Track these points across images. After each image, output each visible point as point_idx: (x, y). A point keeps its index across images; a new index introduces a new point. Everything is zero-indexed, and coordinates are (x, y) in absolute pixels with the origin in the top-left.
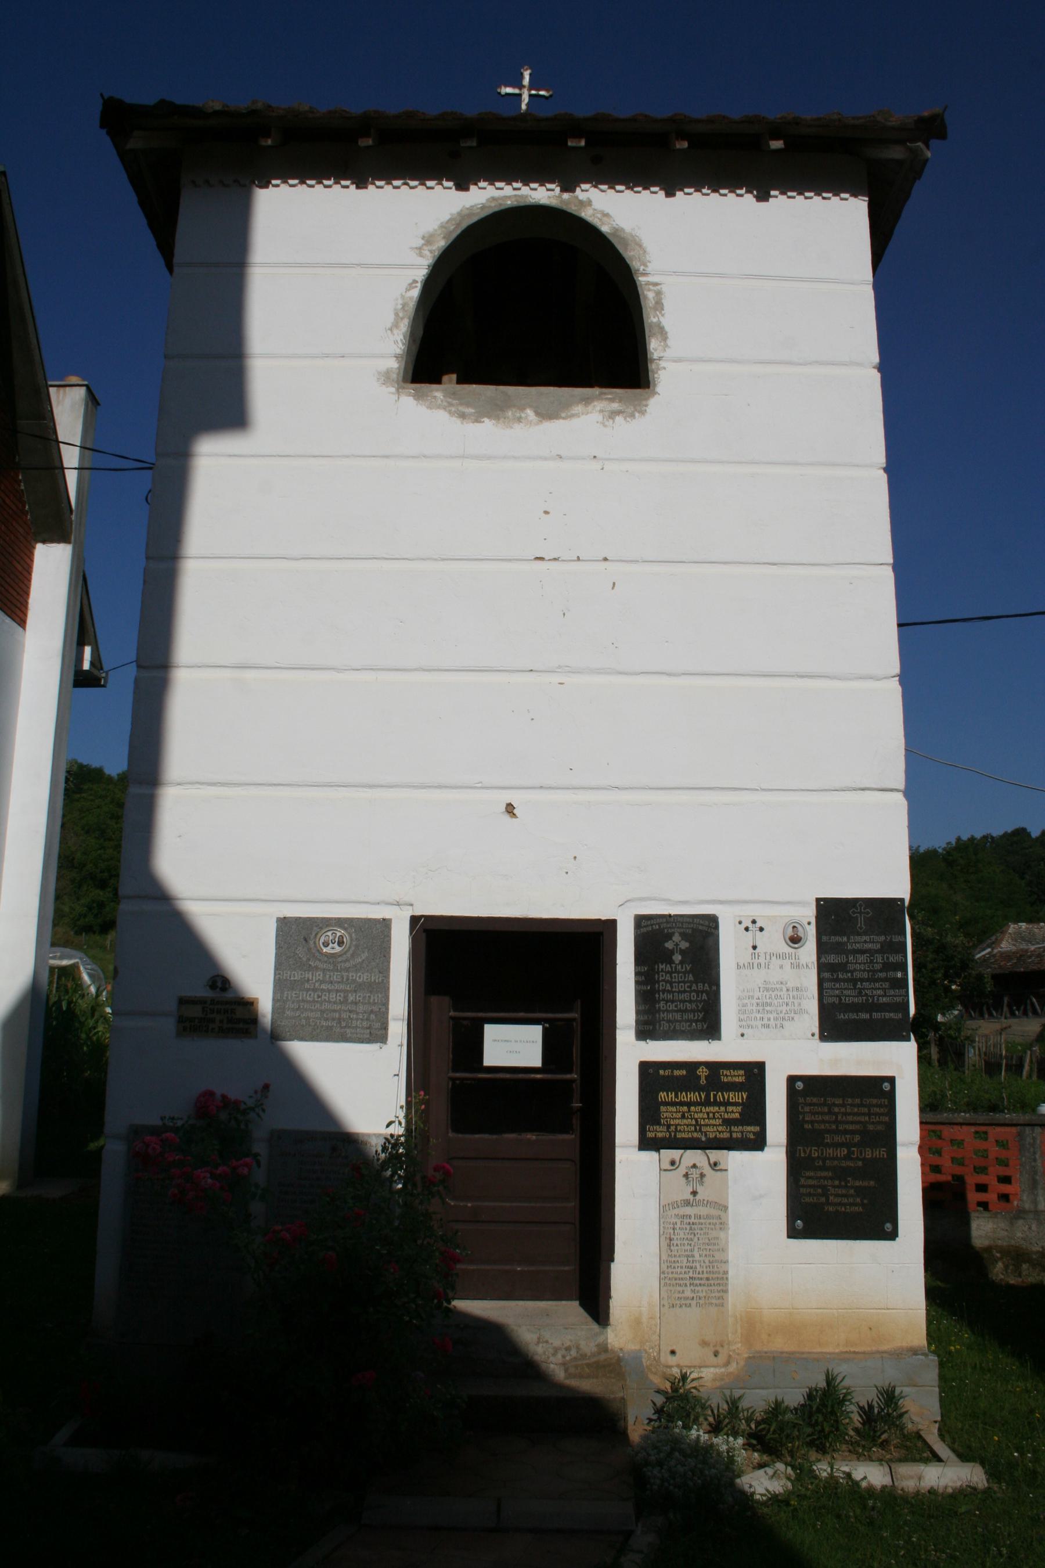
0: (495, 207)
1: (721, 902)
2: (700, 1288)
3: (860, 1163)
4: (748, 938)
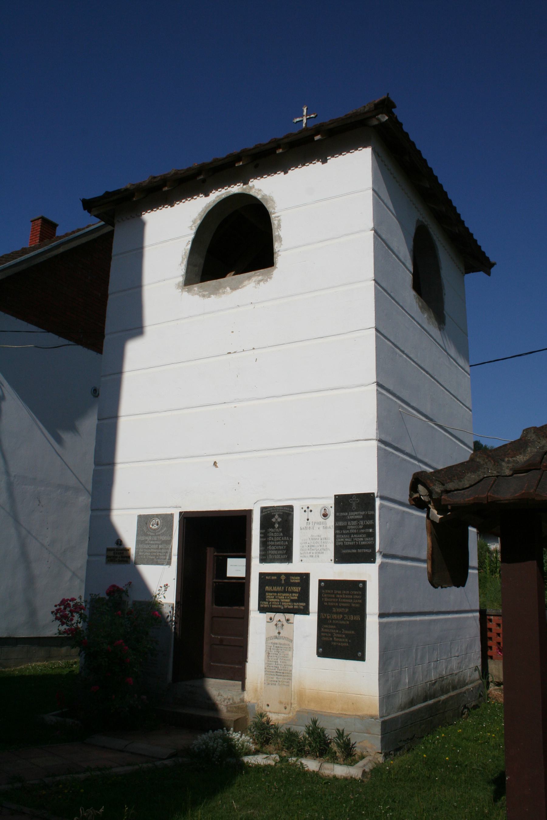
0: (218, 200)
1: (295, 499)
2: (280, 677)
3: (348, 622)
4: (305, 516)
